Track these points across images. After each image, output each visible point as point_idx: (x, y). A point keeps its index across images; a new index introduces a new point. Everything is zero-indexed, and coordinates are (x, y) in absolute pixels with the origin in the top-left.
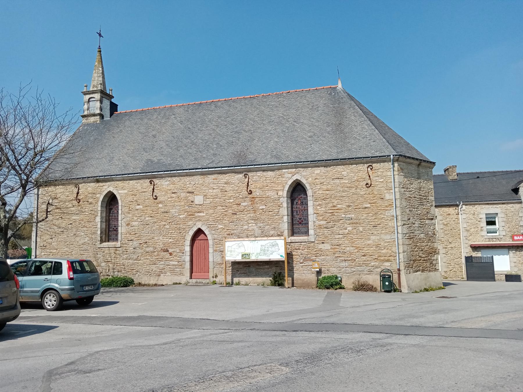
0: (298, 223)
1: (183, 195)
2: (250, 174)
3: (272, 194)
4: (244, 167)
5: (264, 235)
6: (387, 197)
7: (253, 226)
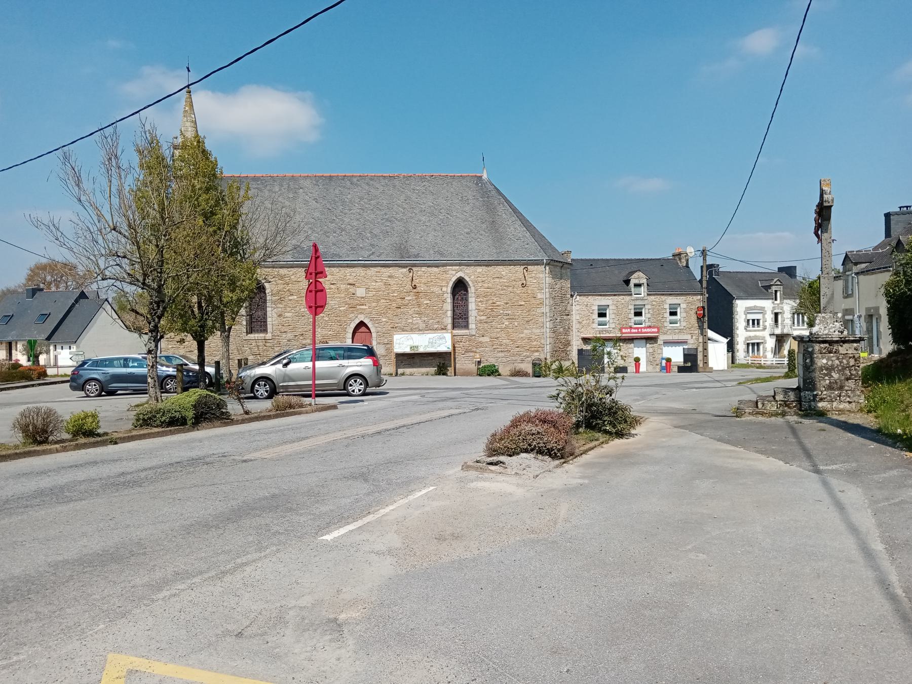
0: (460, 319)
1: (343, 287)
2: (414, 269)
3: (436, 290)
4: (406, 260)
5: (428, 329)
6: (539, 296)
7: (417, 320)
